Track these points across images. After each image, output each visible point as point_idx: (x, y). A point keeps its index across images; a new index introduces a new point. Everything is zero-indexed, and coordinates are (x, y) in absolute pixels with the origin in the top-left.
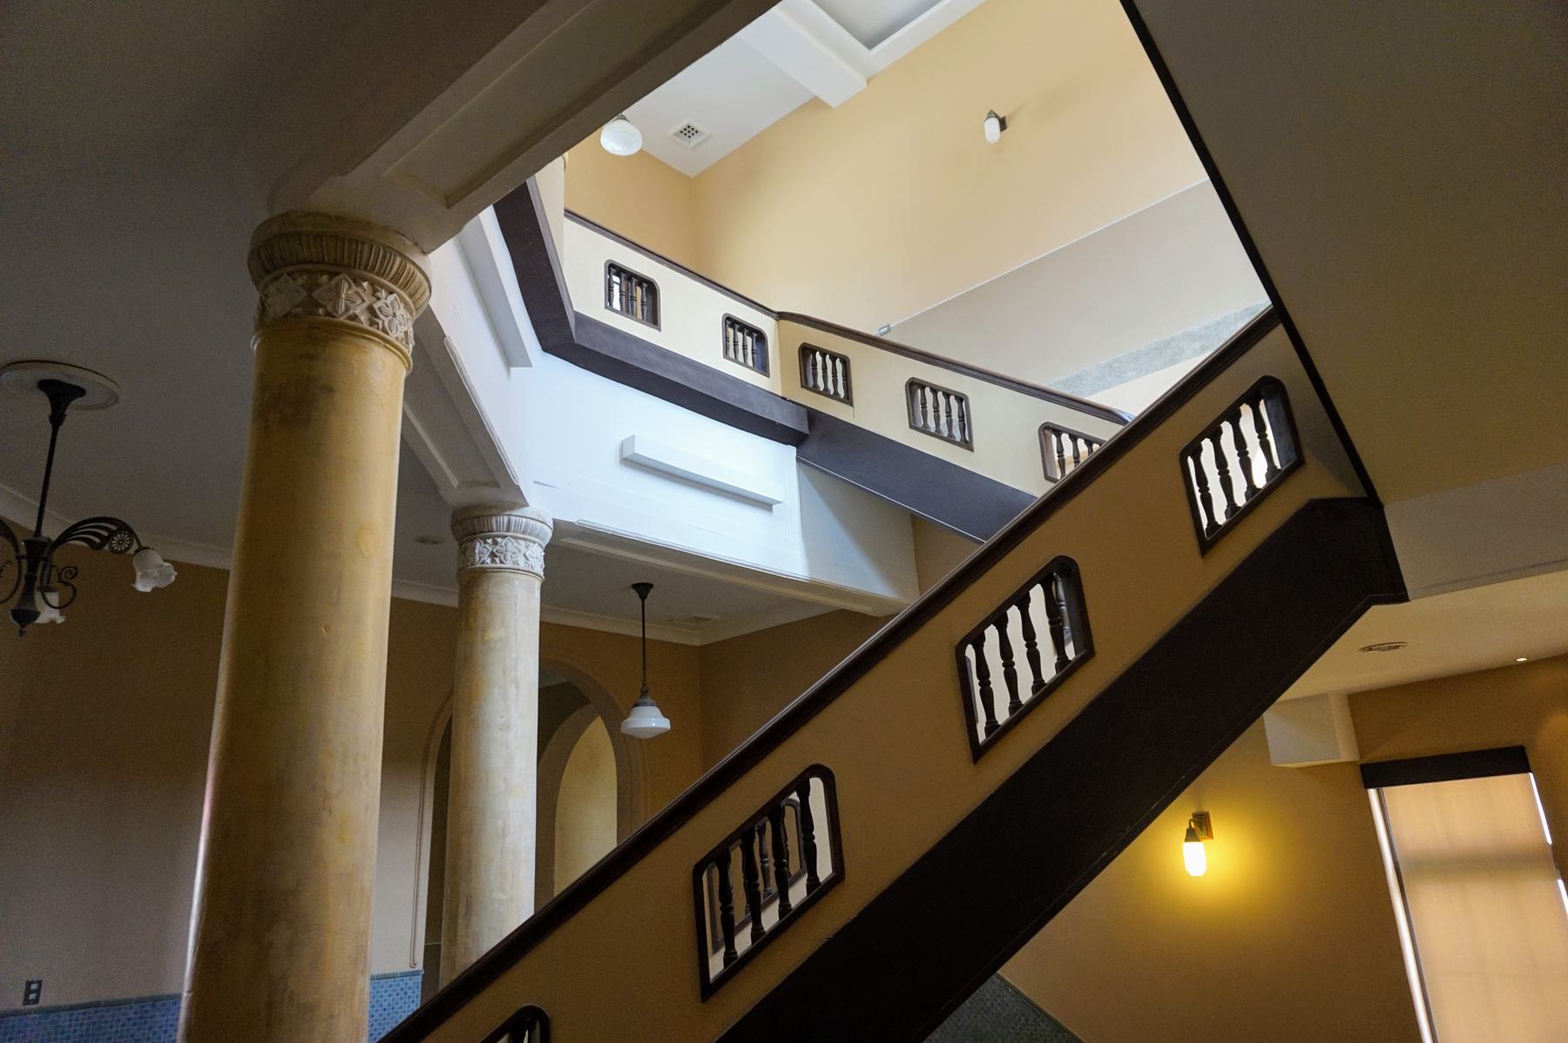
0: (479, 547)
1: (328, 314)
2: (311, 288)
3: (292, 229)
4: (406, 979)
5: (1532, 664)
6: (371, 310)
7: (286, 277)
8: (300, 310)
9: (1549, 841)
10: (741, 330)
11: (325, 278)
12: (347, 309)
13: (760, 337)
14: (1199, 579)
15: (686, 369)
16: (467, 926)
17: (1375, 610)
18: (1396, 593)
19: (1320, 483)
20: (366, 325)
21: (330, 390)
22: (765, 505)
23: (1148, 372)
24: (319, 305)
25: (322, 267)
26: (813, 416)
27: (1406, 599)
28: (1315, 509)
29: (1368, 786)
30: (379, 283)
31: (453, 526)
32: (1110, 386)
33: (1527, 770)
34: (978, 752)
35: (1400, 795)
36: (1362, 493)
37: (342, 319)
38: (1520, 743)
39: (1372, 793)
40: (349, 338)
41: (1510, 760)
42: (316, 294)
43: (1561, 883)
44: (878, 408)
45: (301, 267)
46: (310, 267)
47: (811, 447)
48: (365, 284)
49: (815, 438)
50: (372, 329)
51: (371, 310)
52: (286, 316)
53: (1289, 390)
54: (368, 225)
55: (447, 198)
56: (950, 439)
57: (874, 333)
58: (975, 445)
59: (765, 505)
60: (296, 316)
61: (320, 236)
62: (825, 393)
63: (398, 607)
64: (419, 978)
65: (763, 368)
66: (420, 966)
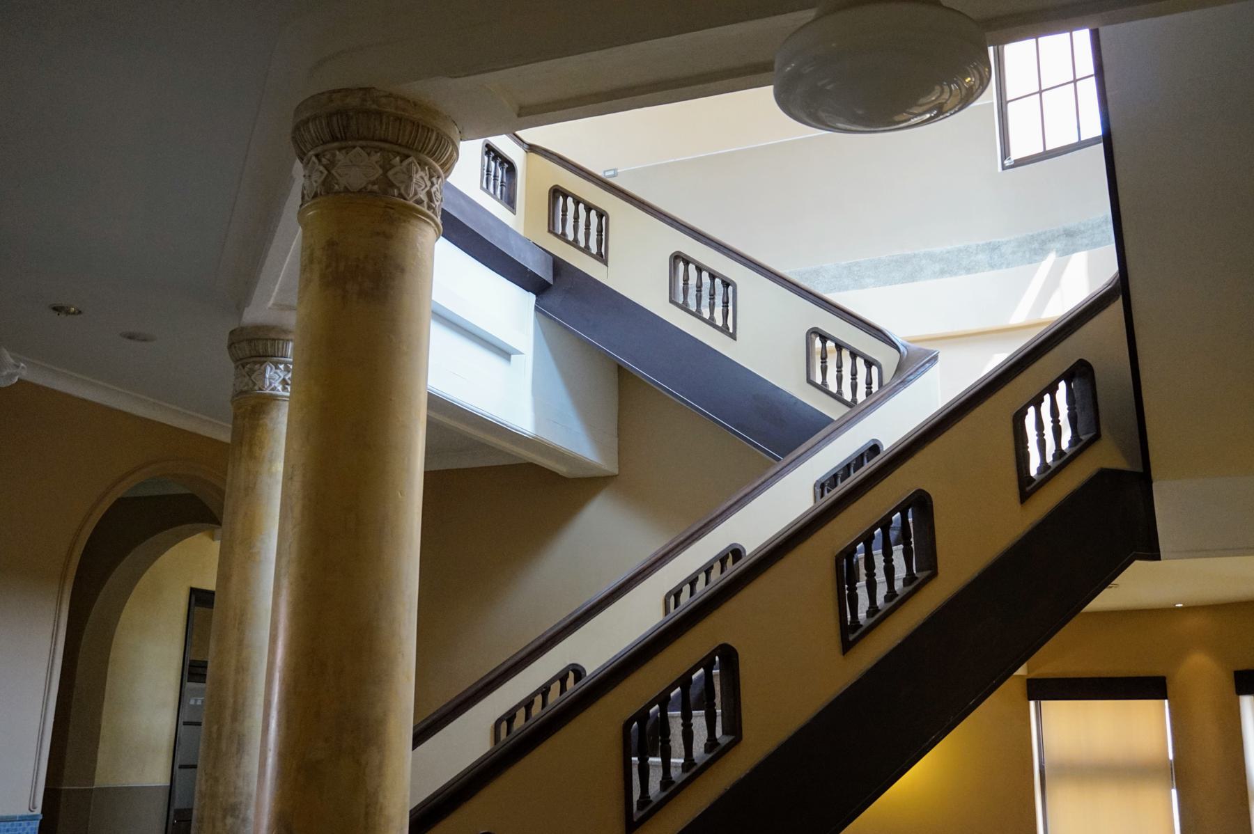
0: (269, 372)
1: (401, 196)
2: (386, 167)
3: (374, 107)
4: (24, 823)
5: (1190, 609)
6: (429, 194)
7: (358, 149)
8: (376, 187)
9: (1171, 757)
10: (495, 159)
11: (257, 366)
12: (416, 194)
13: (511, 169)
14: (1013, 522)
15: (463, 203)
16: (237, 767)
17: (1137, 563)
18: (1153, 554)
19: (1107, 456)
20: (425, 209)
21: (403, 271)
22: (505, 353)
23: (885, 284)
24: (392, 185)
25: (397, 148)
26: (558, 266)
27: (1159, 558)
28: (1104, 477)
29: (1030, 699)
30: (435, 171)
31: (230, 347)
32: (847, 289)
33: (1164, 697)
34: (847, 646)
35: (1053, 708)
36: (1140, 469)
37: (411, 203)
38: (1161, 674)
39: (1032, 703)
40: (414, 222)
41: (1147, 687)
42: (390, 173)
43: (1174, 792)
44: (636, 269)
45: (377, 144)
46: (387, 146)
47: (553, 299)
48: (282, 367)
49: (559, 290)
50: (430, 213)
51: (429, 194)
52: (360, 191)
53: (1097, 375)
54: (437, 112)
55: (521, 108)
56: (711, 322)
57: (600, 173)
58: (738, 335)
59: (505, 353)
60: (372, 192)
61: (399, 119)
62: (575, 243)
63: (427, 474)
64: (36, 824)
65: (510, 202)
66: (38, 811)
